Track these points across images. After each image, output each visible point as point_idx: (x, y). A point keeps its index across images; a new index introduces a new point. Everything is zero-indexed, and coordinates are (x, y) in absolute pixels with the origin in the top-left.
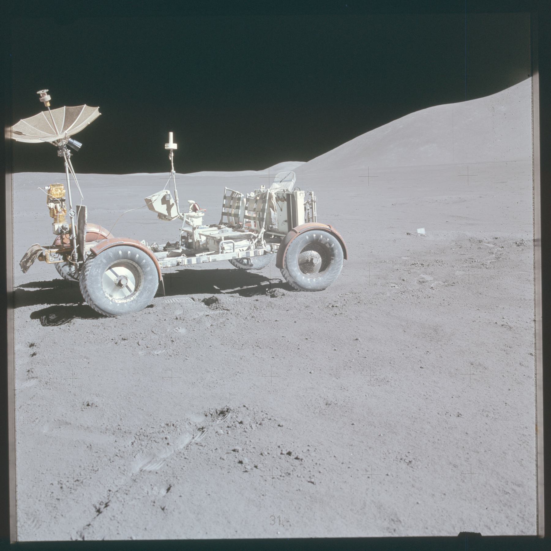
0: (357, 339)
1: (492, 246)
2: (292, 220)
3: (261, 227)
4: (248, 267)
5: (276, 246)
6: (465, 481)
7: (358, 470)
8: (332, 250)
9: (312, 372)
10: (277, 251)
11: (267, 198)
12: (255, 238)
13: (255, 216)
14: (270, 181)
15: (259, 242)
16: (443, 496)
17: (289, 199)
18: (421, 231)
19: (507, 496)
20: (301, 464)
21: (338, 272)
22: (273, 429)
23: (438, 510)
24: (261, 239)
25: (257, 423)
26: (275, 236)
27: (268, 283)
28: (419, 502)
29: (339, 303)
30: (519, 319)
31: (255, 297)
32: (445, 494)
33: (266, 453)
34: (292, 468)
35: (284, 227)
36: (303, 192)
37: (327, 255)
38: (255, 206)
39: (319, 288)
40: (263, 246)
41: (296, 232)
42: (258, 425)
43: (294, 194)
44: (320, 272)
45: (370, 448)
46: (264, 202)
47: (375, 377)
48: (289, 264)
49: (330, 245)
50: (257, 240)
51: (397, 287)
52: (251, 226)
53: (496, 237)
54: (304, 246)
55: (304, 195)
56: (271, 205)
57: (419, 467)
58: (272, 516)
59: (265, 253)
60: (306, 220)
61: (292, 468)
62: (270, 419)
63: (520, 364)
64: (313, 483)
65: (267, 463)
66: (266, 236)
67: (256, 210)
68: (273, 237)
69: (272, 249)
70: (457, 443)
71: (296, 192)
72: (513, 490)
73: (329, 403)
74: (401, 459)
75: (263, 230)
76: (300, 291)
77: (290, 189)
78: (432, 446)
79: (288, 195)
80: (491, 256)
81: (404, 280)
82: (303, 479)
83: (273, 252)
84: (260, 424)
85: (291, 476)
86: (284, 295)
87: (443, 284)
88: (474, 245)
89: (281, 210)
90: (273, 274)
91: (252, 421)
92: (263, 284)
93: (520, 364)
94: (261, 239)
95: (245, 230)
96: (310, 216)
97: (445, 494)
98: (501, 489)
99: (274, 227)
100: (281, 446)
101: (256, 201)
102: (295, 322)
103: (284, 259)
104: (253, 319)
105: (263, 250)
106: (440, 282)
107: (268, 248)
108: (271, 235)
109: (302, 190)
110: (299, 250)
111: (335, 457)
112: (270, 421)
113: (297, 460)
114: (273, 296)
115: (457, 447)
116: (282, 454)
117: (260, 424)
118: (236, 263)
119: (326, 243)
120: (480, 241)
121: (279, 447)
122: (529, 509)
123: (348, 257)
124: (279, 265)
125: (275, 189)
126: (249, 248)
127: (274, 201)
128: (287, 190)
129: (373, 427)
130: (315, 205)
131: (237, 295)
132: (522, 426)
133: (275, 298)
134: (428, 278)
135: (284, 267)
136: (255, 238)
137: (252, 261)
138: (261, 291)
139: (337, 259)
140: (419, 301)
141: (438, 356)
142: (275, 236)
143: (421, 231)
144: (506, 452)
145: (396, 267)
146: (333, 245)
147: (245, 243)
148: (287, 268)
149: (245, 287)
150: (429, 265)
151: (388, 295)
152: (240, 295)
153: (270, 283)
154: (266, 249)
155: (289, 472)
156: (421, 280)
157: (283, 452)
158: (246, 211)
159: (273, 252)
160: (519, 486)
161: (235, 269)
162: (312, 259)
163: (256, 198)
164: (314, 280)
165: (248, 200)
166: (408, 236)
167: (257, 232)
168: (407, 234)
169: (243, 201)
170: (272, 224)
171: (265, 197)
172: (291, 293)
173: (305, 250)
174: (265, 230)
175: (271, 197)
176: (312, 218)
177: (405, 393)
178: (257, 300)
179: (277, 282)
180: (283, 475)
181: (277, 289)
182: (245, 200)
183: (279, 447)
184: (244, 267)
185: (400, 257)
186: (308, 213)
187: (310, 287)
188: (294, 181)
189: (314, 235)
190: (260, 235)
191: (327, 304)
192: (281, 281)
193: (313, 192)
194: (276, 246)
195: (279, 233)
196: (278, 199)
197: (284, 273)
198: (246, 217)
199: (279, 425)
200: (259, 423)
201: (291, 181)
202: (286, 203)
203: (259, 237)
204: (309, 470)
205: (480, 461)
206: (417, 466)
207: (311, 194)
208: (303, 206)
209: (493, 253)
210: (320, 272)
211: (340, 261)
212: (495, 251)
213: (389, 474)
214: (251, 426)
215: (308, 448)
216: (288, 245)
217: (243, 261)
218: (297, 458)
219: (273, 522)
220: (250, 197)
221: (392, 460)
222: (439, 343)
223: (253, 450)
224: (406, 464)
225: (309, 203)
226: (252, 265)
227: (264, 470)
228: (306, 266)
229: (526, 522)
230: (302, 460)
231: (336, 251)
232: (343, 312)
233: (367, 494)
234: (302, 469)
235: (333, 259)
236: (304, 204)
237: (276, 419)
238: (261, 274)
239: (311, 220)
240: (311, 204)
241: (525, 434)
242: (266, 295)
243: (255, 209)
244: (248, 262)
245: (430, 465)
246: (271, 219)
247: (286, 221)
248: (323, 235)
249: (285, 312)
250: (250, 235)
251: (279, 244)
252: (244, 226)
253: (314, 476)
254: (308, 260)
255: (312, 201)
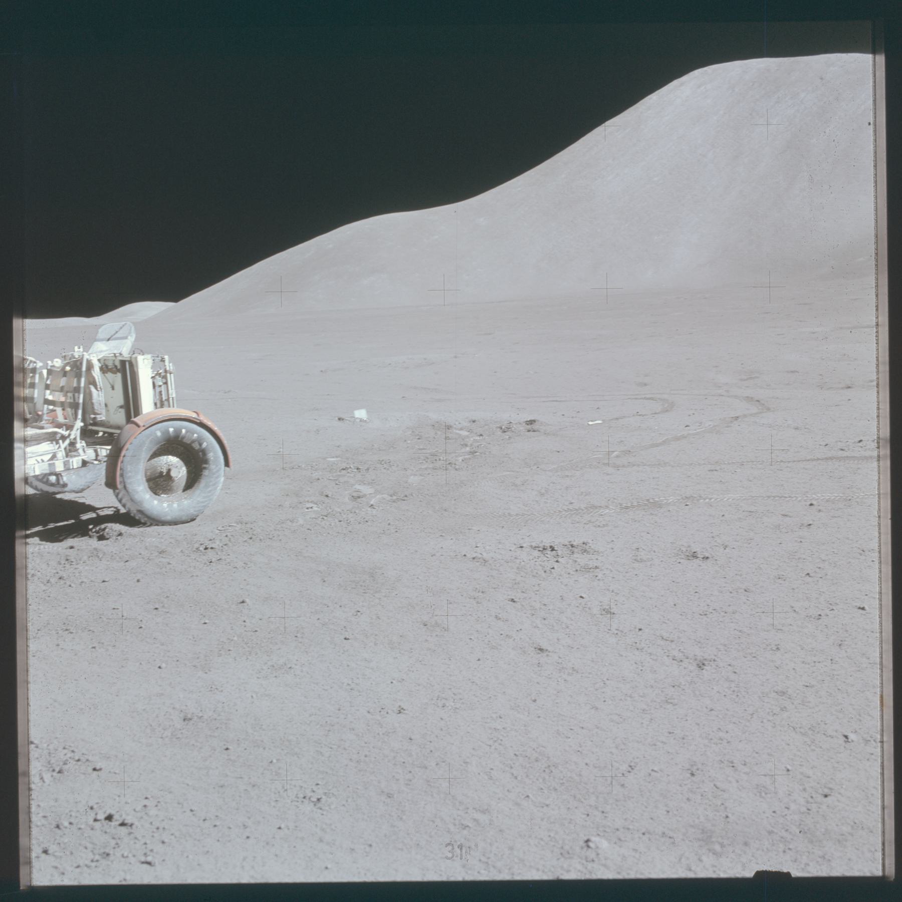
0: (243, 602)
1: (464, 433)
2: (131, 405)
3: (76, 418)
4: (60, 490)
5: (104, 451)
6: (404, 817)
7: (230, 828)
8: (204, 452)
9: (163, 665)
10: (106, 459)
11: (84, 369)
12: (64, 438)
13: (63, 399)
14: (88, 342)
15: (72, 444)
16: (368, 849)
17: (125, 370)
18: (361, 414)
19: (465, 832)
20: (130, 834)
21: (216, 489)
22: (83, 777)
23: (359, 873)
24: (75, 439)
25: (54, 770)
26: (105, 433)
27: (94, 515)
28: (329, 866)
29: (218, 542)
30: (500, 546)
31: (70, 542)
32: (370, 846)
33: (66, 824)
34: (113, 842)
35: (119, 417)
36: (149, 356)
37: (196, 461)
38: (63, 382)
39: (184, 518)
40: (81, 451)
41: (138, 426)
42: (55, 774)
43: (133, 361)
44: (184, 490)
45: (254, 786)
46: (78, 376)
47: (270, 663)
48: (128, 481)
49: (200, 445)
50: (67, 442)
51: (315, 509)
52: (57, 417)
53: (474, 418)
54: (154, 449)
55: (151, 361)
56: (91, 380)
57: (333, 807)
58: (449, 844)
59: (85, 463)
60: (156, 404)
61: (113, 842)
62: (79, 760)
63: (496, 617)
64: (149, 863)
65: (66, 841)
66: (87, 434)
67: (65, 389)
68: (101, 434)
69: (97, 455)
70: (395, 757)
71: (136, 358)
72: (475, 820)
73: (189, 716)
74: (304, 798)
75: (79, 424)
76: (151, 525)
77: (126, 355)
78: (356, 767)
79: (123, 362)
80: (463, 450)
81: (327, 496)
82: (132, 860)
83: (100, 461)
84: (60, 772)
85: (112, 858)
86: (120, 534)
87: (390, 498)
88: (439, 433)
89: (113, 388)
90: (103, 499)
91: (44, 769)
92: (85, 517)
93: (496, 617)
94: (75, 439)
95: (46, 426)
96: (164, 398)
97: (370, 846)
98: (457, 822)
99: (100, 418)
100: (95, 806)
101: (65, 374)
102: (138, 581)
103: (118, 473)
104: (62, 582)
105: (80, 458)
106: (385, 496)
107: (90, 454)
108: (97, 432)
109: (148, 353)
110: (145, 454)
111: (192, 811)
112: (79, 763)
113: (123, 828)
114: (101, 538)
115: (395, 764)
116: (96, 820)
117: (60, 772)
118: (36, 483)
119: (193, 442)
120: (449, 427)
121: (92, 808)
122: (498, 848)
123: (231, 464)
124: (111, 483)
125: (98, 353)
126: (54, 457)
127: (96, 373)
128: (121, 354)
129: (261, 749)
130: (171, 378)
131: (36, 540)
132: (494, 716)
133: (104, 542)
134: (366, 490)
135: (119, 486)
136: (64, 438)
137: (65, 479)
138: (81, 530)
139: (212, 467)
140: (350, 528)
141: (374, 617)
142: (105, 433)
143: (361, 414)
144: (468, 760)
145: (316, 475)
146: (204, 445)
147: (46, 447)
148: (125, 487)
149: (51, 526)
150: (368, 469)
151: (301, 522)
152: (41, 540)
153: (97, 514)
154: (85, 458)
155: (107, 851)
156: (355, 494)
157: (99, 817)
158: (48, 392)
159: (100, 461)
160: (484, 812)
161: (35, 494)
162: (169, 471)
163: (63, 368)
164: (175, 505)
165: (50, 372)
166: (340, 423)
167: (70, 427)
168: (339, 419)
169: (41, 374)
170: (95, 414)
171: (81, 364)
172: (135, 530)
173: (155, 455)
174: (82, 424)
175: (90, 366)
176: (168, 400)
177: (317, 684)
178: (72, 547)
179: (110, 512)
180: (97, 857)
181: (109, 525)
182: (45, 372)
183: (92, 808)
184: (51, 489)
185: (325, 459)
186: (161, 392)
187: (169, 518)
188: (131, 339)
189: (171, 430)
190: (73, 433)
191: (197, 545)
192: (118, 510)
193: (166, 357)
194: (104, 451)
195: (111, 427)
196: (105, 369)
197: (120, 496)
198: (47, 402)
199: (95, 769)
200: (57, 769)
201: (126, 338)
202: (119, 375)
203: (72, 437)
204: (143, 841)
205: (428, 781)
206: (329, 805)
207: (163, 360)
208: (151, 381)
209: (466, 445)
210: (184, 490)
211: (218, 471)
212: (470, 441)
213: (283, 826)
214: (42, 778)
215: (146, 802)
216: (126, 447)
217: (48, 479)
218: (123, 824)
219: (450, 855)
220: (53, 366)
221: (289, 801)
222: (377, 595)
223: (44, 821)
224: (312, 804)
225: (161, 376)
226: (65, 485)
227: (61, 854)
228: (160, 483)
229: (492, 869)
230: (131, 825)
231: (211, 456)
232: (223, 558)
233: (243, 867)
234: (132, 842)
235: (205, 468)
236: (152, 377)
237: (90, 758)
238: (81, 501)
239: (166, 403)
240: (165, 377)
241: (499, 727)
242: (90, 537)
243: (62, 387)
244: (58, 480)
245: (350, 800)
246: (92, 404)
247: (121, 407)
248: (185, 429)
249: (122, 564)
250: (55, 433)
251: (109, 447)
252: (45, 417)
253: (152, 851)
254: (161, 473)
255: (166, 371)
